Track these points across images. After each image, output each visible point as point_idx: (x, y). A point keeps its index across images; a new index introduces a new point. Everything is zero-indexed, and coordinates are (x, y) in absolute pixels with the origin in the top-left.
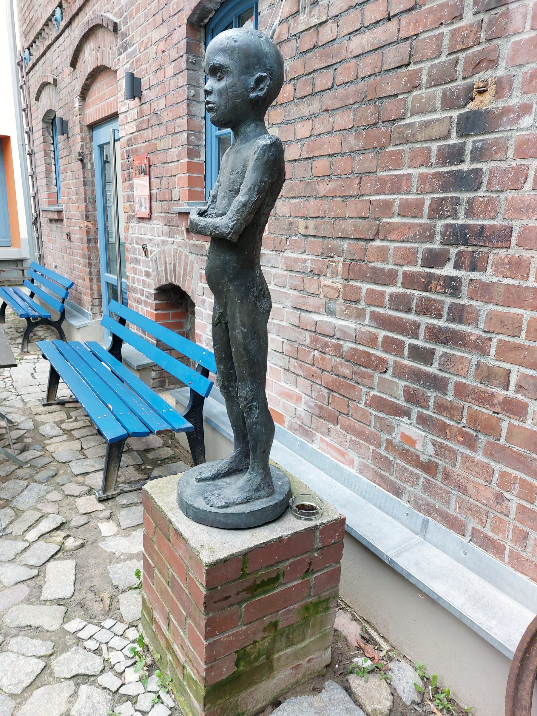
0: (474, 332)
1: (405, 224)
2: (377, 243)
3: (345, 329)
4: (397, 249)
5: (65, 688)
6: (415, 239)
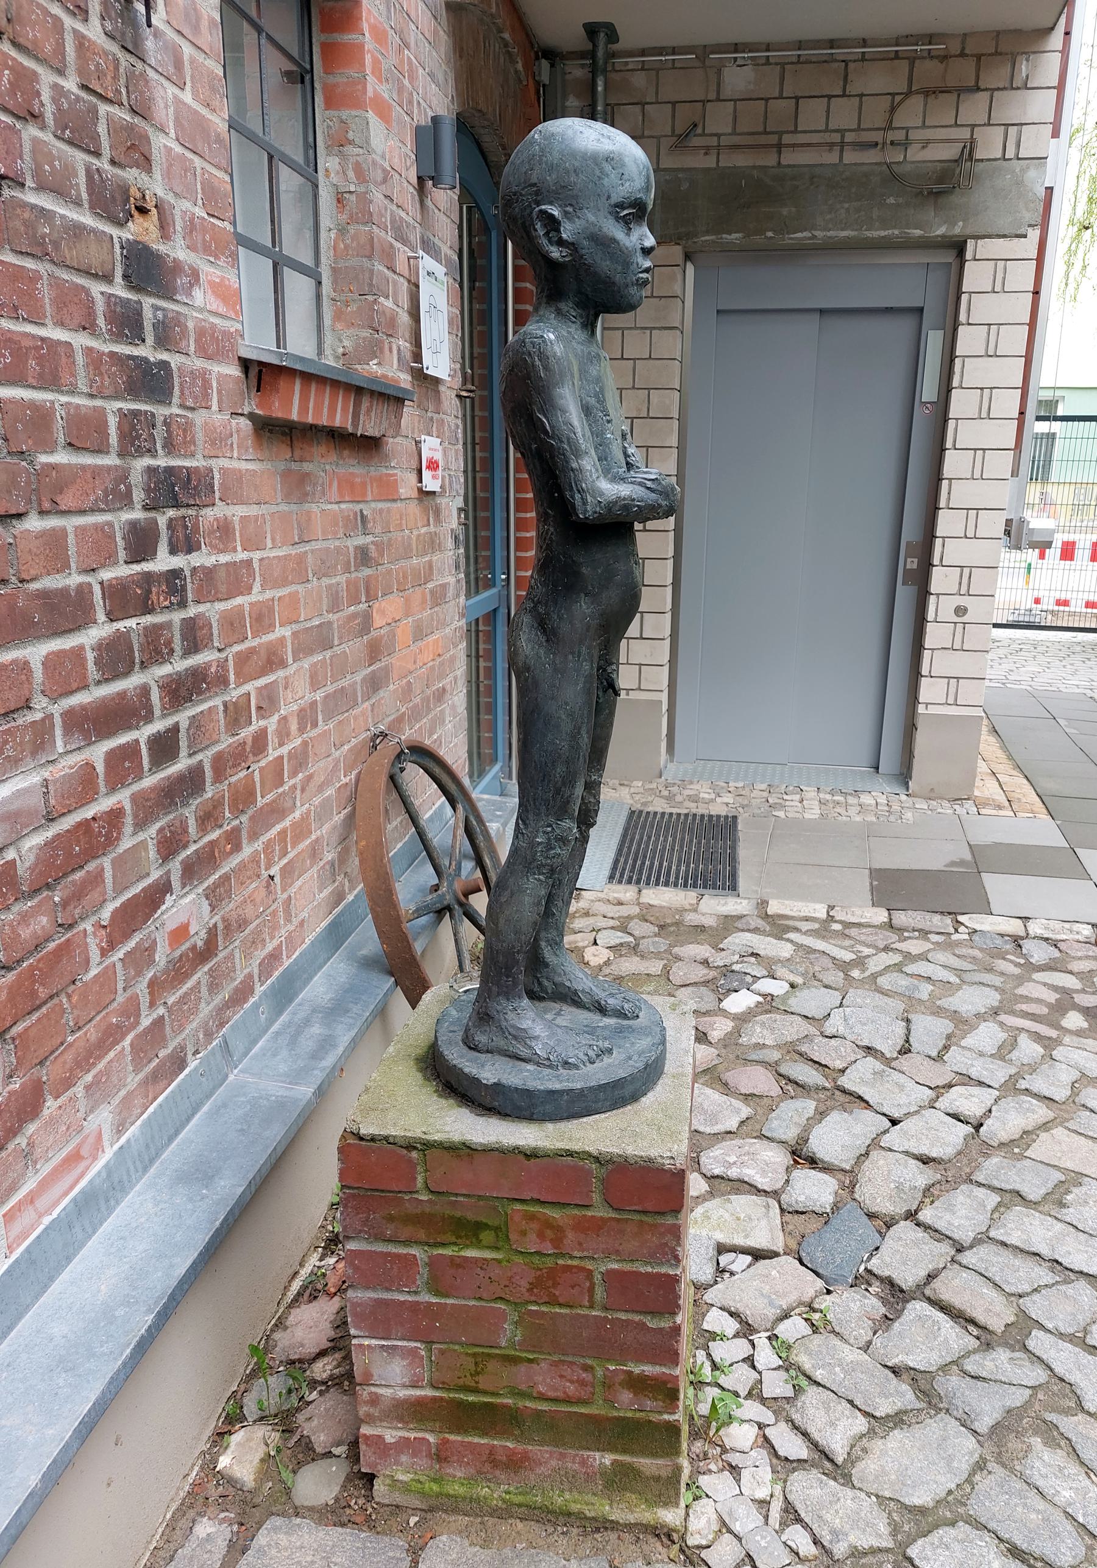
0: (209, 658)
1: (83, 468)
2: (34, 523)
3: (14, 807)
4: (80, 531)
5: (871, 1478)
6: (107, 503)
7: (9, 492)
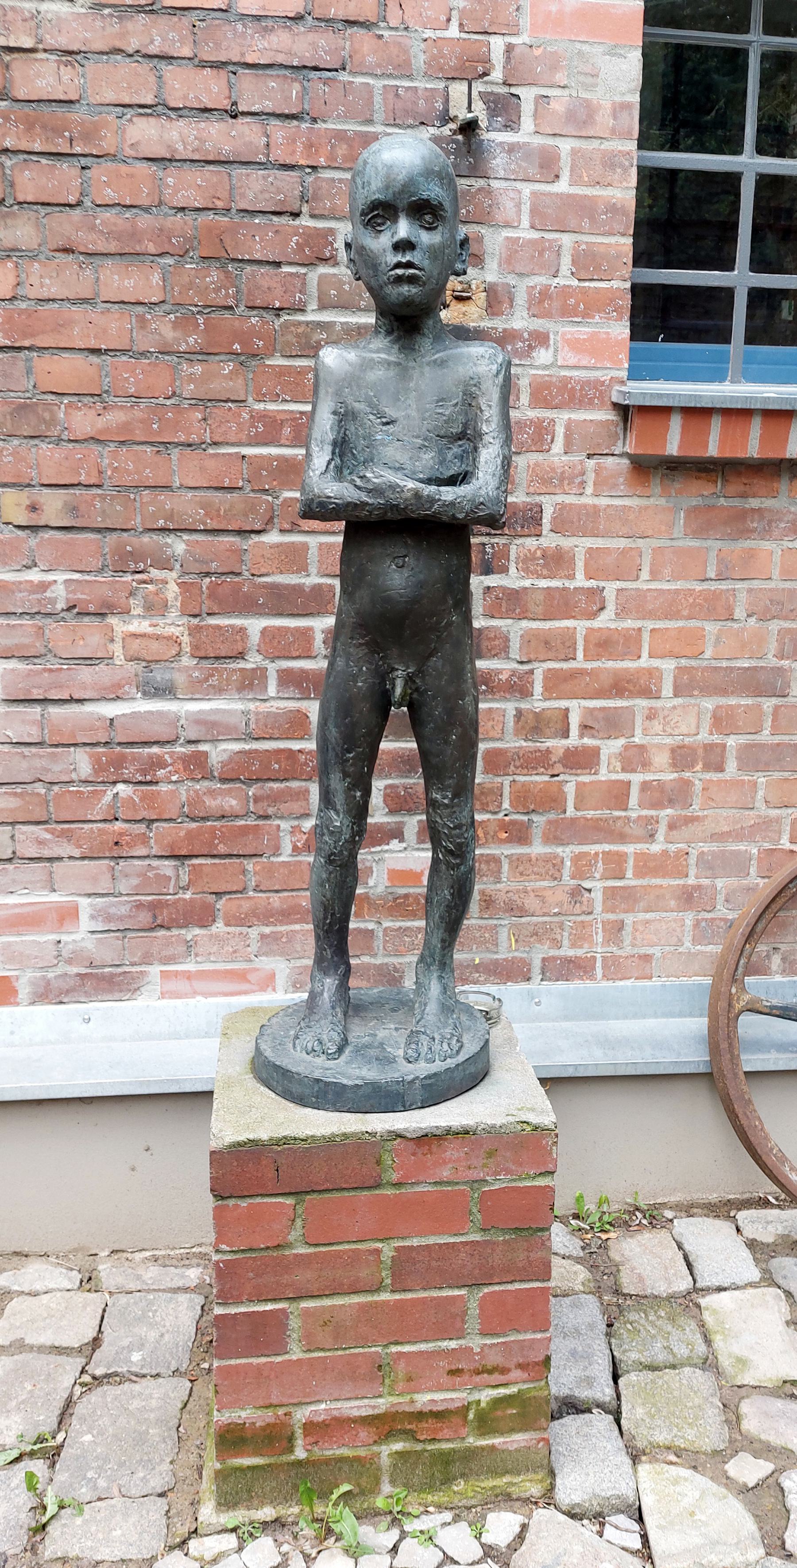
2: (273, 538)
3: (212, 718)
7: (247, 516)
